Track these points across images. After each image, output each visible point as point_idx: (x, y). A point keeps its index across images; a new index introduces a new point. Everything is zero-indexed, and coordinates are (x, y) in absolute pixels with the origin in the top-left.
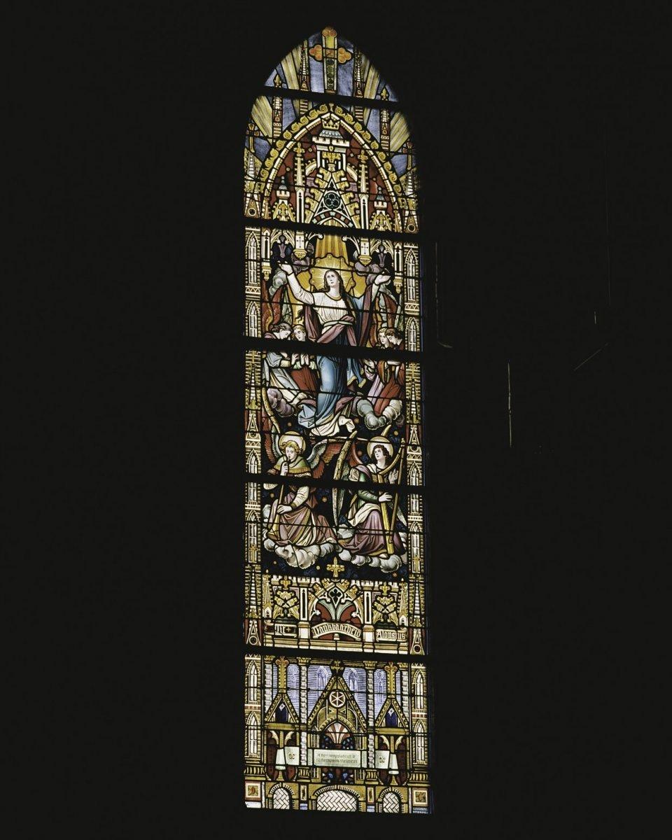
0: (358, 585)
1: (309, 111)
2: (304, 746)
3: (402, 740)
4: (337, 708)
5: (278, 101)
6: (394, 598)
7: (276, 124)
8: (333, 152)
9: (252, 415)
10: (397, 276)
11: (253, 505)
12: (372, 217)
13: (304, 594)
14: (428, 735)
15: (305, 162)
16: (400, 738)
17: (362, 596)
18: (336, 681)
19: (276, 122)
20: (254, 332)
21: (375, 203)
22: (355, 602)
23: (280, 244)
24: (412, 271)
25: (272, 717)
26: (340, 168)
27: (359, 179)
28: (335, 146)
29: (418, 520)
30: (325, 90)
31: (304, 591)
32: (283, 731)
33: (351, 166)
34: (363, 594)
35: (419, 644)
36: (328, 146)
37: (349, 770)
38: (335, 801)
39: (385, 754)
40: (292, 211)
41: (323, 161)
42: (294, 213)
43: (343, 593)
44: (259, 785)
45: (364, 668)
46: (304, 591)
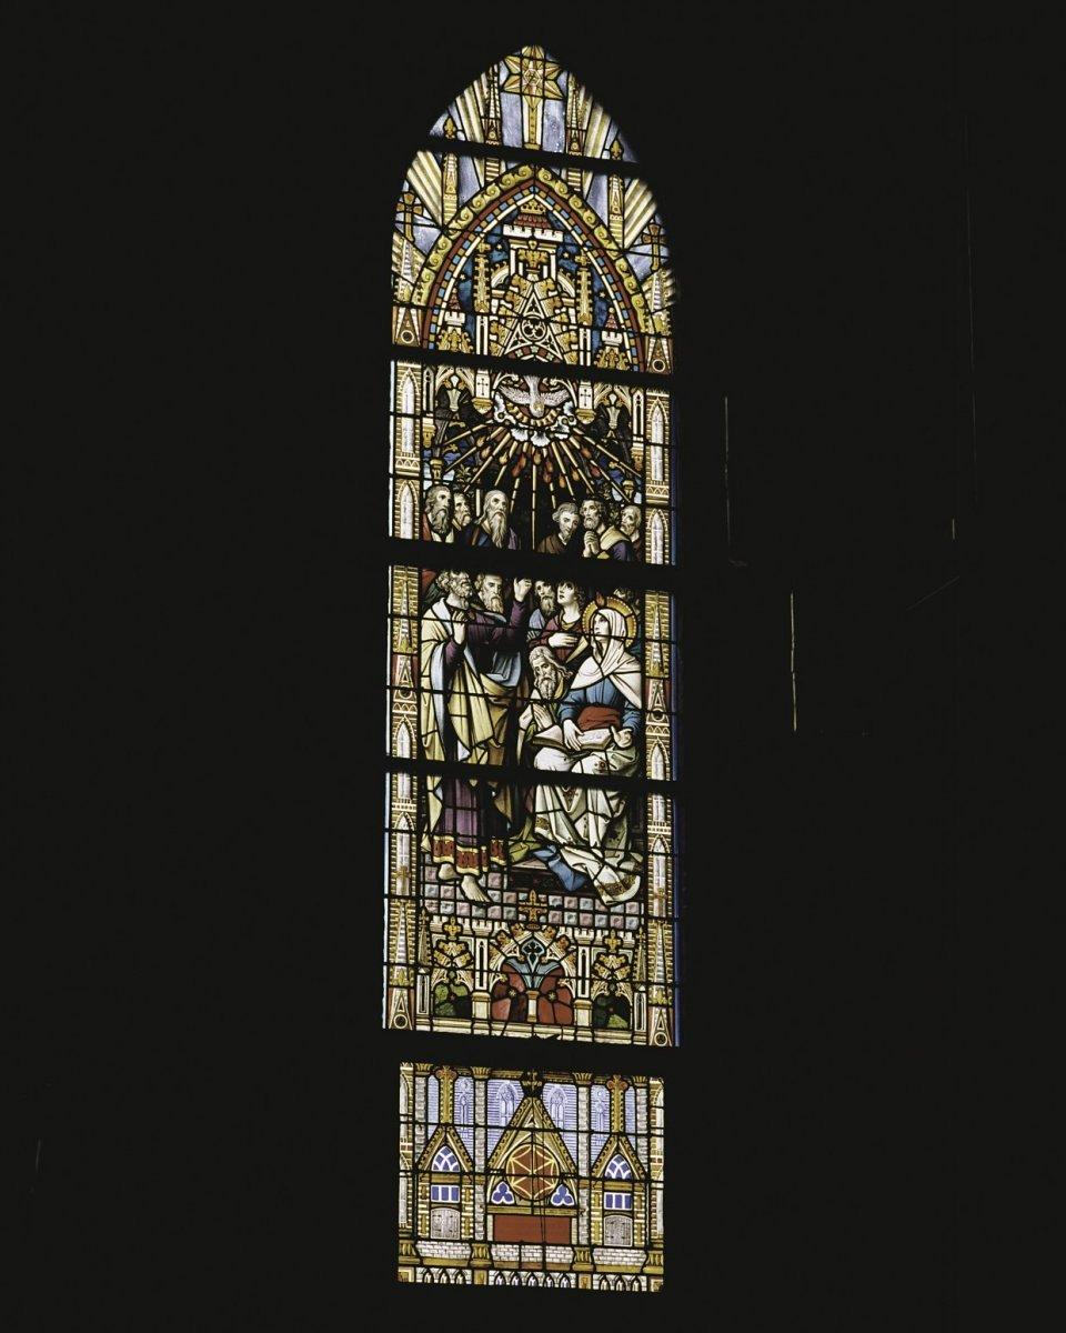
0: (570, 935)
1: (501, 176)
5: (451, 160)
6: (626, 958)
8: (536, 250)
9: (401, 661)
10: (637, 442)
11: (404, 804)
12: (598, 356)
13: (482, 950)
15: (492, 266)
17: (575, 954)
18: (529, 1166)
21: (604, 333)
22: (563, 963)
23: (451, 389)
24: (657, 434)
26: (545, 275)
27: (578, 295)
28: (539, 241)
29: (408, 810)
30: (524, 143)
31: (482, 943)
33: (565, 273)
34: (577, 950)
36: (527, 240)
40: (469, 344)
41: (521, 265)
42: (472, 348)
43: (546, 949)
45: (472, 1076)
46: (482, 943)
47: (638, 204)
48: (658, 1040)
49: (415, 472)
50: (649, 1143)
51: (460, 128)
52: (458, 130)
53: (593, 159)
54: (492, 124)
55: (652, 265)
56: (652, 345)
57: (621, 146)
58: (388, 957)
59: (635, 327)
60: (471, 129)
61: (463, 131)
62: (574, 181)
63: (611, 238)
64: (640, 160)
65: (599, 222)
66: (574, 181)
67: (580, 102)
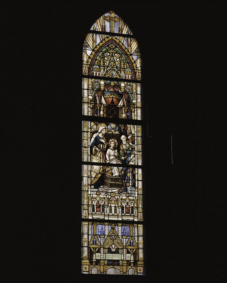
2: (102, 252)
3: (98, 249)
4: (113, 240)
7: (94, 43)
14: (144, 248)
16: (97, 249)
18: (112, 221)
19: (94, 42)
20: (85, 160)
25: (91, 243)
30: (110, 31)
32: (133, 249)
35: (141, 218)
37: (118, 261)
38: (111, 271)
39: (129, 255)
44: (88, 266)
47: (134, 48)
48: (85, 217)
49: (87, 101)
50: (138, 238)
51: (97, 28)
52: (96, 29)
53: (124, 34)
54: (104, 27)
55: (137, 57)
56: (137, 74)
57: (130, 32)
58: (83, 130)
59: (133, 67)
60: (99, 29)
61: (97, 29)
62: (120, 39)
63: (128, 51)
64: (136, 34)
65: (126, 48)
66: (120, 39)
67: (122, 23)
